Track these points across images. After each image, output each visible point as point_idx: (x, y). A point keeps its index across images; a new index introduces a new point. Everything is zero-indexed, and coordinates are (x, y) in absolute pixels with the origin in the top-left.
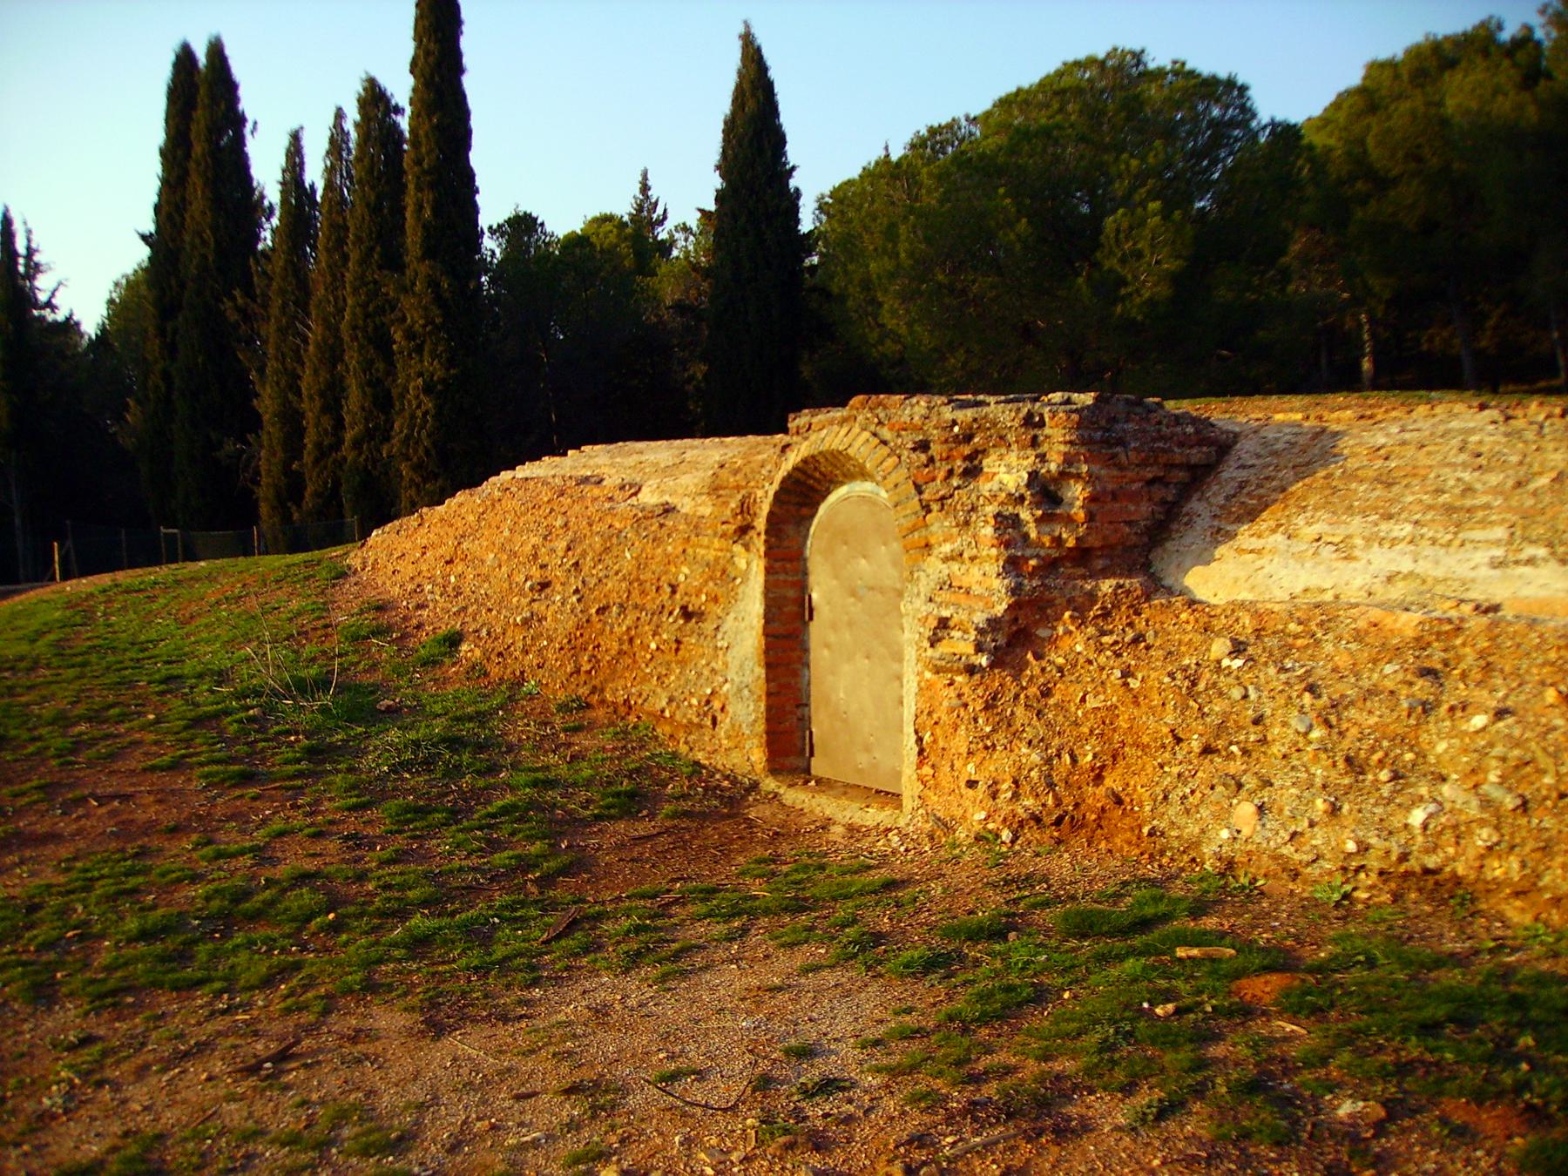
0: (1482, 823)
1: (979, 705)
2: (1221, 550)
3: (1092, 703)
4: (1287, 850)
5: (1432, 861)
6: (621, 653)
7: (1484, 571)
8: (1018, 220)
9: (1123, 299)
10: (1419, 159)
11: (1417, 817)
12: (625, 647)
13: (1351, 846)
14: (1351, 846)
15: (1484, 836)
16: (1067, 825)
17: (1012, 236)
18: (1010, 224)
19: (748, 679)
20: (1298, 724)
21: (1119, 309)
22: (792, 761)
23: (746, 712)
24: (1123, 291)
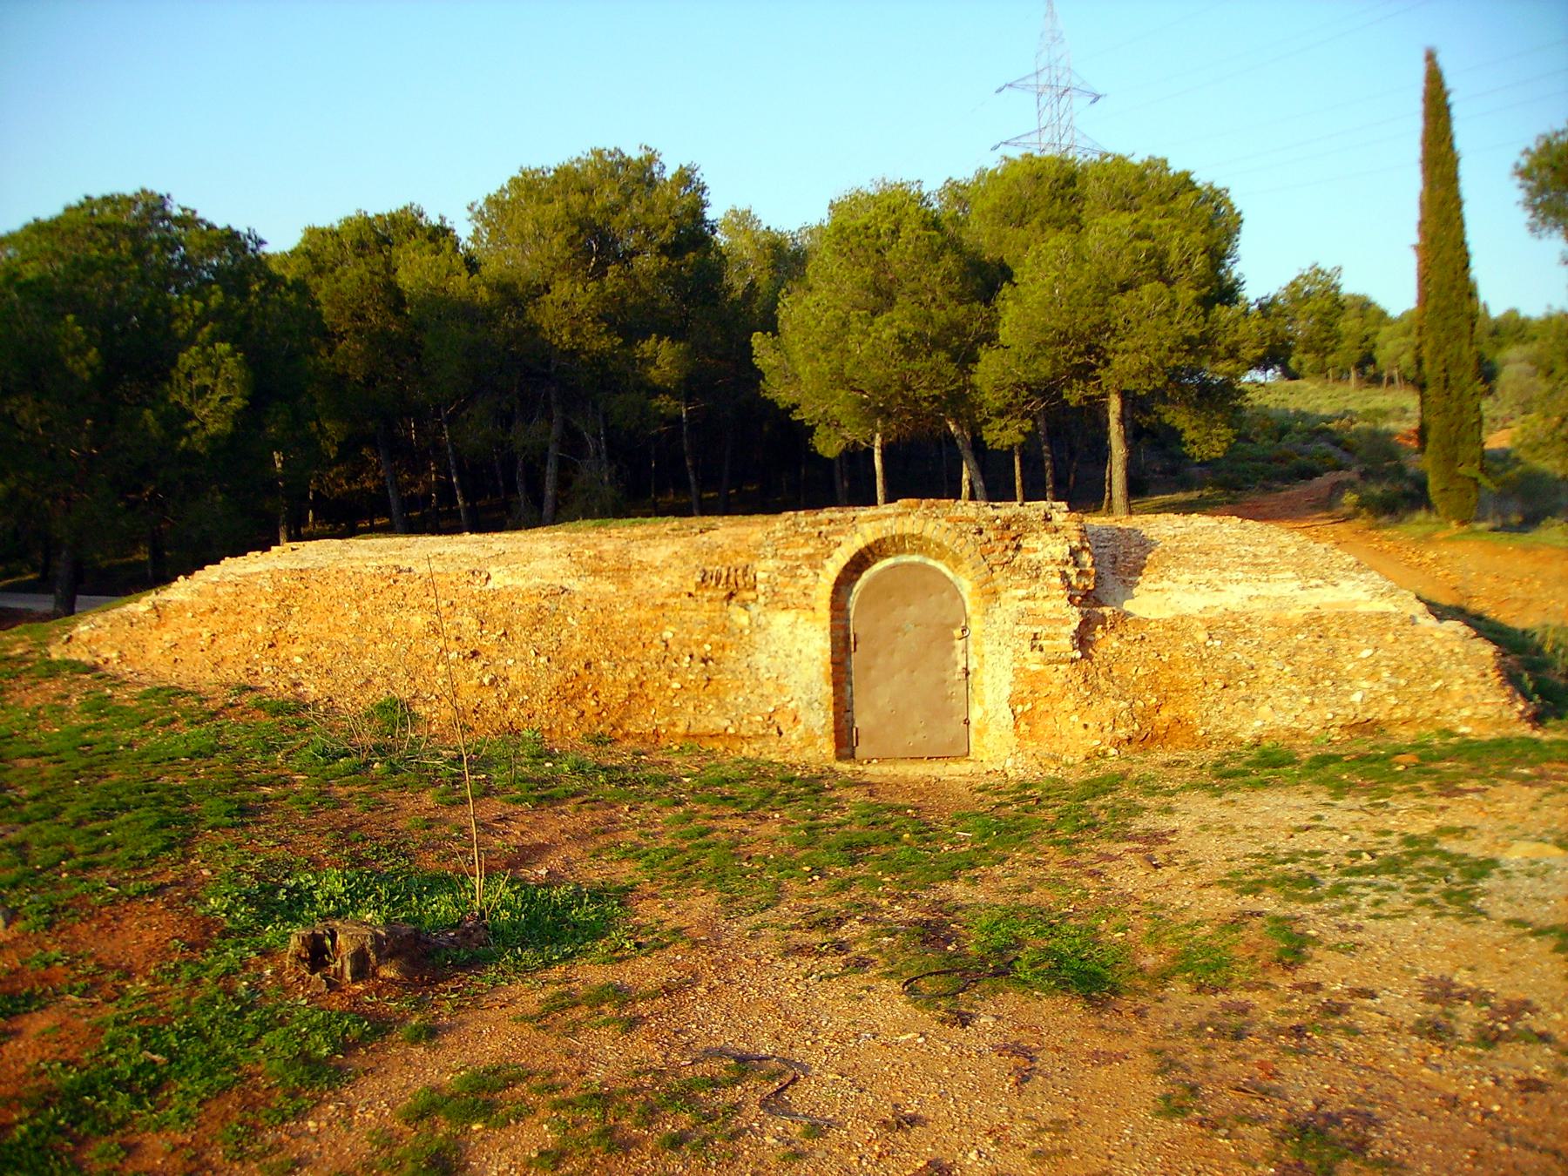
0: (1389, 694)
1: (1081, 679)
2: (1135, 591)
3: (1141, 672)
4: (1295, 725)
5: (1369, 716)
6: (631, 696)
7: (1298, 592)
8: (89, 349)
9: (187, 434)
10: (361, 318)
11: (1357, 697)
12: (637, 690)
13: (1330, 716)
14: (1330, 716)
15: (1392, 700)
16: (1144, 741)
17: (83, 364)
18: (79, 351)
19: (817, 695)
20: (1275, 666)
21: (183, 442)
22: (847, 751)
23: (820, 720)
24: (189, 425)
